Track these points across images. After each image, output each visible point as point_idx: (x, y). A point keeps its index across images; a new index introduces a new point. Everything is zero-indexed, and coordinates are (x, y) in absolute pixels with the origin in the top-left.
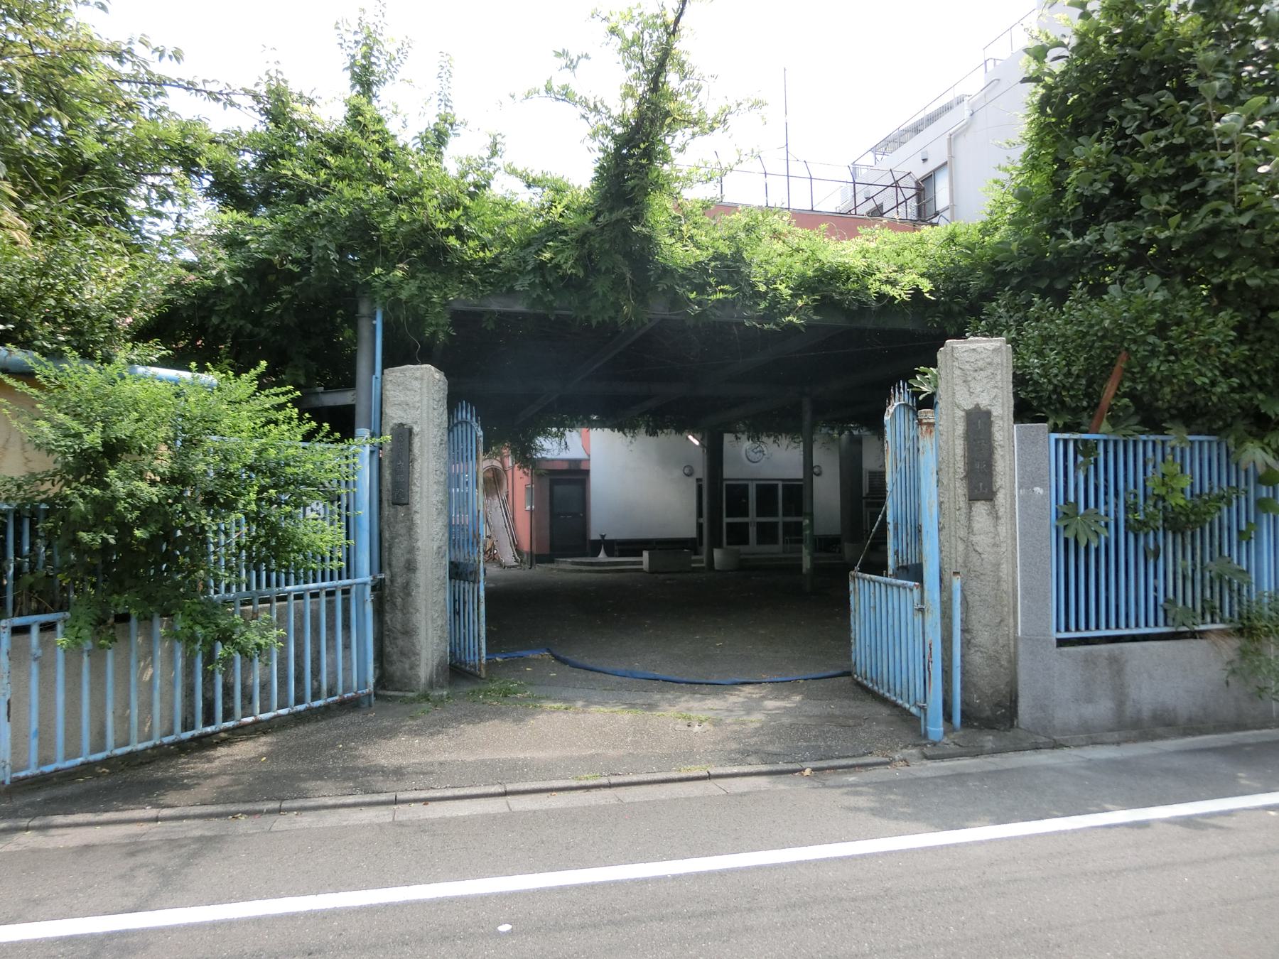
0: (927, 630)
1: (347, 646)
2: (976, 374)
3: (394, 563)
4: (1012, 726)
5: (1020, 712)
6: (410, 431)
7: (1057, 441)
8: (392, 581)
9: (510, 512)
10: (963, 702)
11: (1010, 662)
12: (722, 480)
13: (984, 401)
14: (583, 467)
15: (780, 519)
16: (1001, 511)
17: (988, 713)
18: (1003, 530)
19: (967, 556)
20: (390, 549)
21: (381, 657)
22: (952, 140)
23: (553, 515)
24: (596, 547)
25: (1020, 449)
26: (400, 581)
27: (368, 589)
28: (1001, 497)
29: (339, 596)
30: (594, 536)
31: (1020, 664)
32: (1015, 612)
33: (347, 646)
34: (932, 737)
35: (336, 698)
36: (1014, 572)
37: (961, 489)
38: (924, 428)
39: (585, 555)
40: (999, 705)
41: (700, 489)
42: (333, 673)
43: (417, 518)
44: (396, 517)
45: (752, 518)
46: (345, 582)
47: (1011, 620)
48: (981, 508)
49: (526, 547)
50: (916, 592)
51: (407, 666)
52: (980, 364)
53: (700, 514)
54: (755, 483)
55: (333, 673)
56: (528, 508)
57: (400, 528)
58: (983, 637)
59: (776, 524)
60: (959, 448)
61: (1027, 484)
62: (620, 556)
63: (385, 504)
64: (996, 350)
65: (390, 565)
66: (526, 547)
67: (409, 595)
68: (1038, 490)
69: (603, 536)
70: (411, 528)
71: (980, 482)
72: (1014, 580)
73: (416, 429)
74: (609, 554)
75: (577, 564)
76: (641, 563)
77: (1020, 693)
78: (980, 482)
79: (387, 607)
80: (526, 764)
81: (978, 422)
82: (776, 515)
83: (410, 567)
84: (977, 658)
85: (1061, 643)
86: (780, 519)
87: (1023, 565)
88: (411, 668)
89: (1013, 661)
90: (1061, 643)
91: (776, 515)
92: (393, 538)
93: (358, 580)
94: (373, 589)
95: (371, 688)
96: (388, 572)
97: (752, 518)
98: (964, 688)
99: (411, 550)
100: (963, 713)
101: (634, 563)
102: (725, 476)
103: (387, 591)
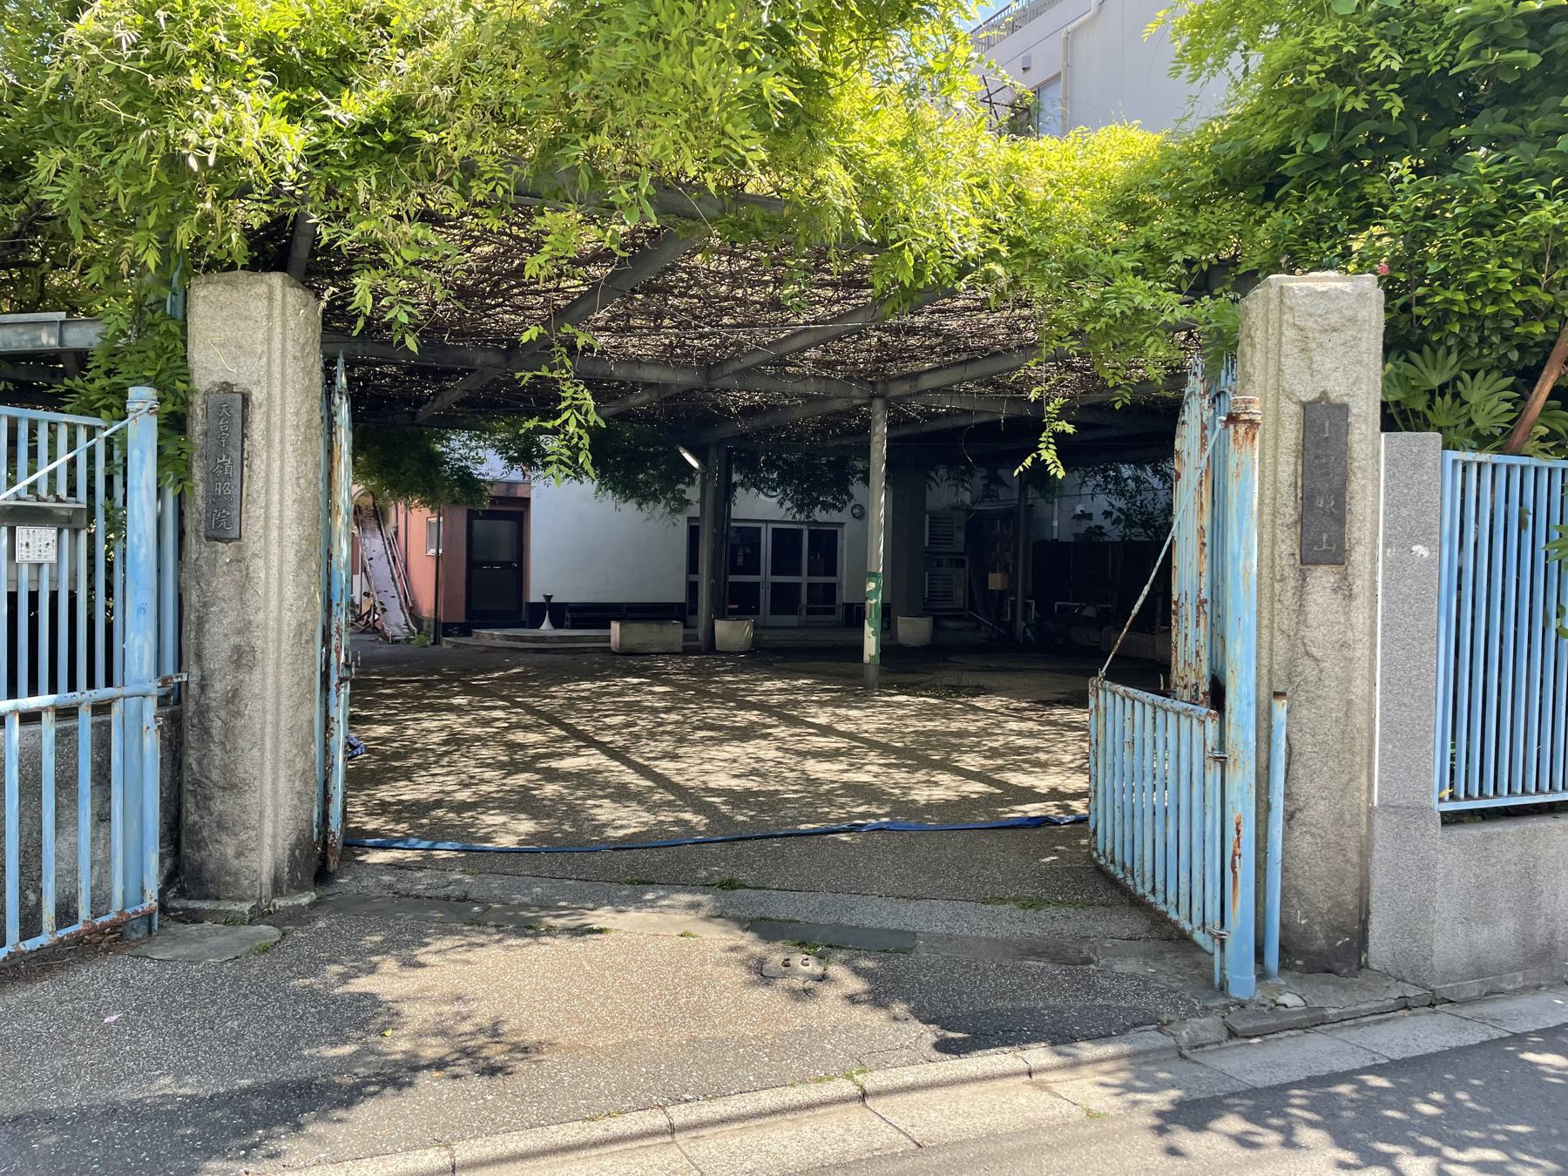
0: (1230, 797)
1: (103, 818)
2: (1324, 338)
3: (208, 650)
4: (1360, 967)
5: (1371, 942)
6: (246, 398)
7: (1455, 462)
8: (203, 688)
9: (399, 557)
10: (1283, 926)
11: (1361, 854)
12: (729, 519)
13: (1337, 390)
14: (520, 493)
15: (804, 579)
16: (1360, 585)
17: (1321, 943)
18: (1360, 618)
19: (1292, 663)
20: (201, 622)
21: (175, 831)
22: (1070, 40)
23: (471, 564)
24: (536, 613)
25: (1390, 476)
26: (219, 687)
27: (151, 705)
28: (1359, 556)
29: (85, 720)
30: (535, 595)
31: (1376, 856)
32: (1370, 765)
33: (103, 818)
34: (1236, 992)
35: (79, 927)
36: (1371, 694)
37: (1287, 545)
38: (1242, 429)
39: (521, 625)
40: (1341, 930)
41: (694, 533)
42: (69, 874)
43: (258, 568)
44: (213, 564)
45: (766, 577)
46: (102, 693)
47: (1364, 779)
48: (1322, 579)
49: (426, 606)
50: (1212, 727)
51: (230, 852)
52: (1334, 319)
53: (693, 566)
54: (771, 526)
55: (69, 874)
56: (433, 551)
57: (223, 585)
58: (1317, 811)
59: (798, 586)
60: (1287, 468)
61: (1400, 539)
62: (573, 627)
63: (191, 539)
64: (1362, 296)
65: (199, 657)
66: (426, 606)
67: (238, 714)
68: (1420, 550)
69: (548, 598)
70: (245, 584)
71: (1321, 532)
72: (1371, 705)
73: (257, 396)
74: (557, 624)
75: (516, 638)
76: (608, 639)
77: (1374, 906)
78: (1321, 532)
79: (191, 737)
80: (223, 526)
81: (1322, 425)
82: (798, 573)
83: (242, 658)
84: (1305, 844)
85: (1450, 819)
86: (804, 579)
87: (1387, 681)
88: (239, 855)
89: (1365, 852)
90: (1450, 819)
91: (798, 573)
92: (205, 605)
93: (127, 691)
94: (162, 701)
95: (151, 901)
96: (194, 670)
97: (766, 577)
98: (1285, 902)
99: (245, 628)
100: (1283, 948)
101: (595, 639)
102: (733, 516)
103: (191, 707)
